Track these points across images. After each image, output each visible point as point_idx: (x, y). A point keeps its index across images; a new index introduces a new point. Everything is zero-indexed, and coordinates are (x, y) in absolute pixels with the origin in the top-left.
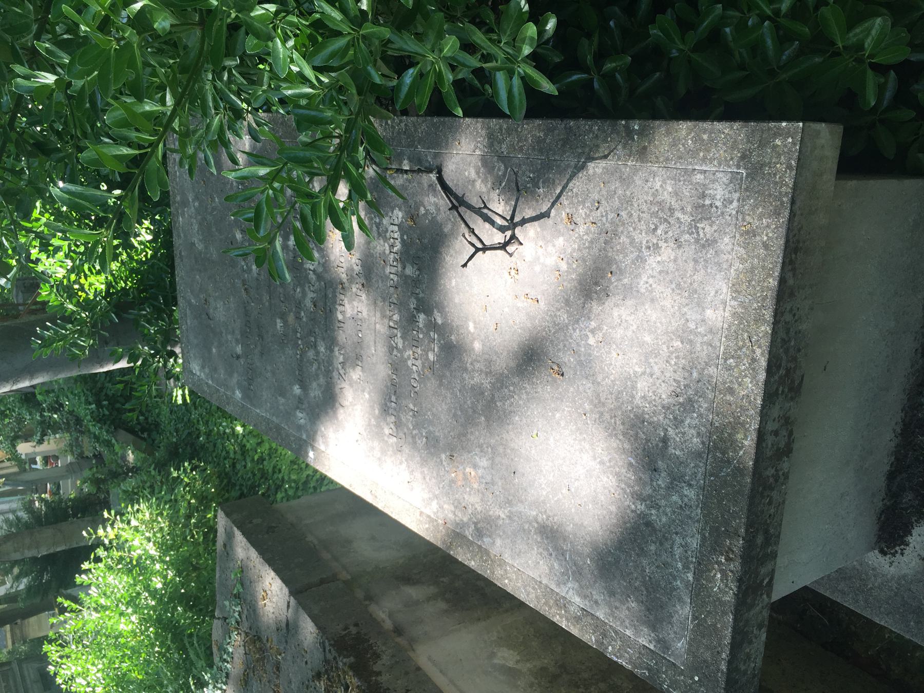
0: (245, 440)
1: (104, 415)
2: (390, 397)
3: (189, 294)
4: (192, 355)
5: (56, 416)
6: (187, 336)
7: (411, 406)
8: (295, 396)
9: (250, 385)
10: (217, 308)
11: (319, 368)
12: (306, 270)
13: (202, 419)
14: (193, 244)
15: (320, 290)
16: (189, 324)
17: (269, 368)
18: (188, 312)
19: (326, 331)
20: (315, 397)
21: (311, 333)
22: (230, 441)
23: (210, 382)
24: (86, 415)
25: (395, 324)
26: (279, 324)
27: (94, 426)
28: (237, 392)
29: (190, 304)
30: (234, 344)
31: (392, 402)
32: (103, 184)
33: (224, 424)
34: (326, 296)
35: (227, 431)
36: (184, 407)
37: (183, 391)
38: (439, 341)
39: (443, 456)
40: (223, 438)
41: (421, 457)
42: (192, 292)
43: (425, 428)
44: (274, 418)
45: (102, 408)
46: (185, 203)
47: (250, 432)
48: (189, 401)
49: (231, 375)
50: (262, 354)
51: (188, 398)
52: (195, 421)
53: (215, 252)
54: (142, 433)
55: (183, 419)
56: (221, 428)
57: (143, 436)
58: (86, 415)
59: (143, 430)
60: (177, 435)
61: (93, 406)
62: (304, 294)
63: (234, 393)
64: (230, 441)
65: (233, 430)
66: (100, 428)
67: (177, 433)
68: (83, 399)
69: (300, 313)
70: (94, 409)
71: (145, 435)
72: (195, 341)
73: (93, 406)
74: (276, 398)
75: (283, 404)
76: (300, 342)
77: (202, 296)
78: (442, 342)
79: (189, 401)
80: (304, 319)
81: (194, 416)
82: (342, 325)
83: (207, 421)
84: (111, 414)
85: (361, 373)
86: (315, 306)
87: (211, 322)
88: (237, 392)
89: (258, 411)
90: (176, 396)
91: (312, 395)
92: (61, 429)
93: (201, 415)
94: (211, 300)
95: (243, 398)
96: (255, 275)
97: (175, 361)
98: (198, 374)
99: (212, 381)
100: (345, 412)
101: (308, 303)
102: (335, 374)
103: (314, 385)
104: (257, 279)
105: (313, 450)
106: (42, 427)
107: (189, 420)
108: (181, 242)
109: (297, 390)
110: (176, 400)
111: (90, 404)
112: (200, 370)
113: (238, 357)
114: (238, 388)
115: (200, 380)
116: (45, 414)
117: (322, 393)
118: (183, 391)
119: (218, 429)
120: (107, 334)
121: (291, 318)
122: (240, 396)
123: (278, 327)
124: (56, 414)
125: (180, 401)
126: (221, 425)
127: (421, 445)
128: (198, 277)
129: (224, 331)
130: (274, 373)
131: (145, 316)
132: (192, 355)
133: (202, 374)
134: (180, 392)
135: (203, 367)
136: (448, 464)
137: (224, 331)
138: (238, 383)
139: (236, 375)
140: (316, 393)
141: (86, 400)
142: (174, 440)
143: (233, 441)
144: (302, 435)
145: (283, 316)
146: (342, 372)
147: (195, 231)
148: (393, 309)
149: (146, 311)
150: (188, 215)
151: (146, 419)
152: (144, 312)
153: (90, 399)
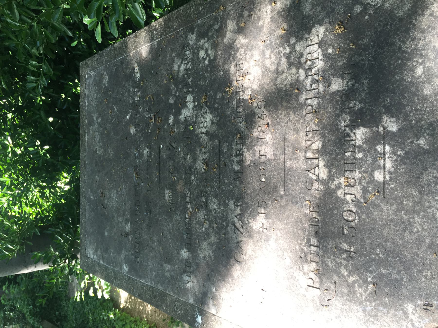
0: (115, 323)
1: (37, 312)
2: (309, 240)
3: (90, 192)
4: (88, 242)
5: (12, 314)
6: (85, 227)
7: (345, 246)
8: (182, 260)
9: (136, 257)
10: (110, 197)
11: (210, 226)
12: (198, 135)
13: (91, 311)
14: (95, 152)
15: (213, 148)
16: (87, 217)
17: (155, 238)
18: (88, 207)
19: (219, 187)
20: (205, 257)
21: (202, 193)
22: (106, 324)
23: (101, 262)
24: (27, 312)
25: (314, 154)
26: (168, 194)
27: (31, 318)
28: (124, 267)
29: (89, 200)
30: (124, 224)
31: (311, 245)
32: (38, 141)
33: (103, 314)
34: (220, 152)
35: (105, 318)
36: (81, 305)
37: (81, 293)
38: (394, 153)
39: (410, 307)
40: (102, 323)
41: (364, 311)
42: (91, 191)
43: (370, 272)
44: (159, 285)
45: (36, 308)
46: (91, 123)
47: (119, 318)
48: (83, 300)
49: (119, 252)
50: (149, 227)
51: (83, 297)
52: (87, 313)
53: (112, 152)
54: (57, 322)
55: (80, 312)
56: (101, 316)
57: (57, 324)
58: (27, 312)
59: (57, 321)
60: (76, 322)
61: (31, 307)
62: (195, 159)
63: (121, 268)
64: (106, 324)
65: (108, 317)
66: (34, 320)
67: (76, 321)
68: (26, 302)
69: (190, 178)
70: (31, 309)
71: (59, 323)
72: (91, 230)
73: (31, 307)
74: (162, 265)
75: (169, 271)
76: (189, 206)
77: (99, 191)
78: (400, 152)
79: (83, 300)
80: (195, 183)
81: (87, 309)
82: (239, 175)
83: (94, 313)
84: (41, 311)
85: (264, 221)
86: (207, 166)
87: (105, 210)
88: (124, 267)
89: (143, 281)
90: (77, 296)
91: (202, 256)
92: (14, 321)
93: (90, 309)
94: (107, 193)
95: (129, 272)
96: (146, 158)
97: (76, 262)
98: (92, 257)
99: (103, 261)
100: (242, 268)
101: (200, 166)
102: (230, 229)
103: (205, 245)
104: (148, 161)
105: (201, 314)
106: (4, 321)
107: (83, 312)
108: (85, 154)
109: (185, 254)
110: (76, 299)
111: (30, 305)
112: (94, 254)
113: (127, 234)
114: (125, 263)
115: (93, 261)
116: (6, 313)
117: (213, 252)
118: (81, 293)
119: (100, 317)
120: (31, 244)
121: (180, 186)
122: (127, 269)
123: (167, 198)
124: (12, 313)
125: (78, 299)
126: (101, 314)
127: (365, 295)
128: (97, 177)
129: (116, 215)
130: (160, 242)
131: (59, 232)
132: (88, 242)
133: (95, 257)
134: (79, 294)
135: (96, 250)
136: (420, 317)
137: (116, 215)
138: (125, 258)
139: (124, 251)
140: (206, 253)
141: (28, 303)
142: (74, 325)
143: (108, 324)
144: (188, 299)
145: (172, 187)
146: (238, 225)
147: (97, 141)
148: (313, 137)
149: (60, 229)
150: (93, 131)
151: (60, 313)
152: (59, 230)
153: (30, 303)
